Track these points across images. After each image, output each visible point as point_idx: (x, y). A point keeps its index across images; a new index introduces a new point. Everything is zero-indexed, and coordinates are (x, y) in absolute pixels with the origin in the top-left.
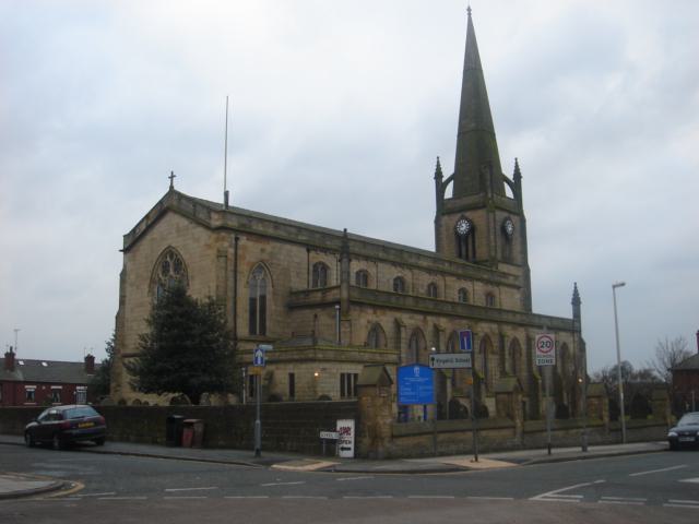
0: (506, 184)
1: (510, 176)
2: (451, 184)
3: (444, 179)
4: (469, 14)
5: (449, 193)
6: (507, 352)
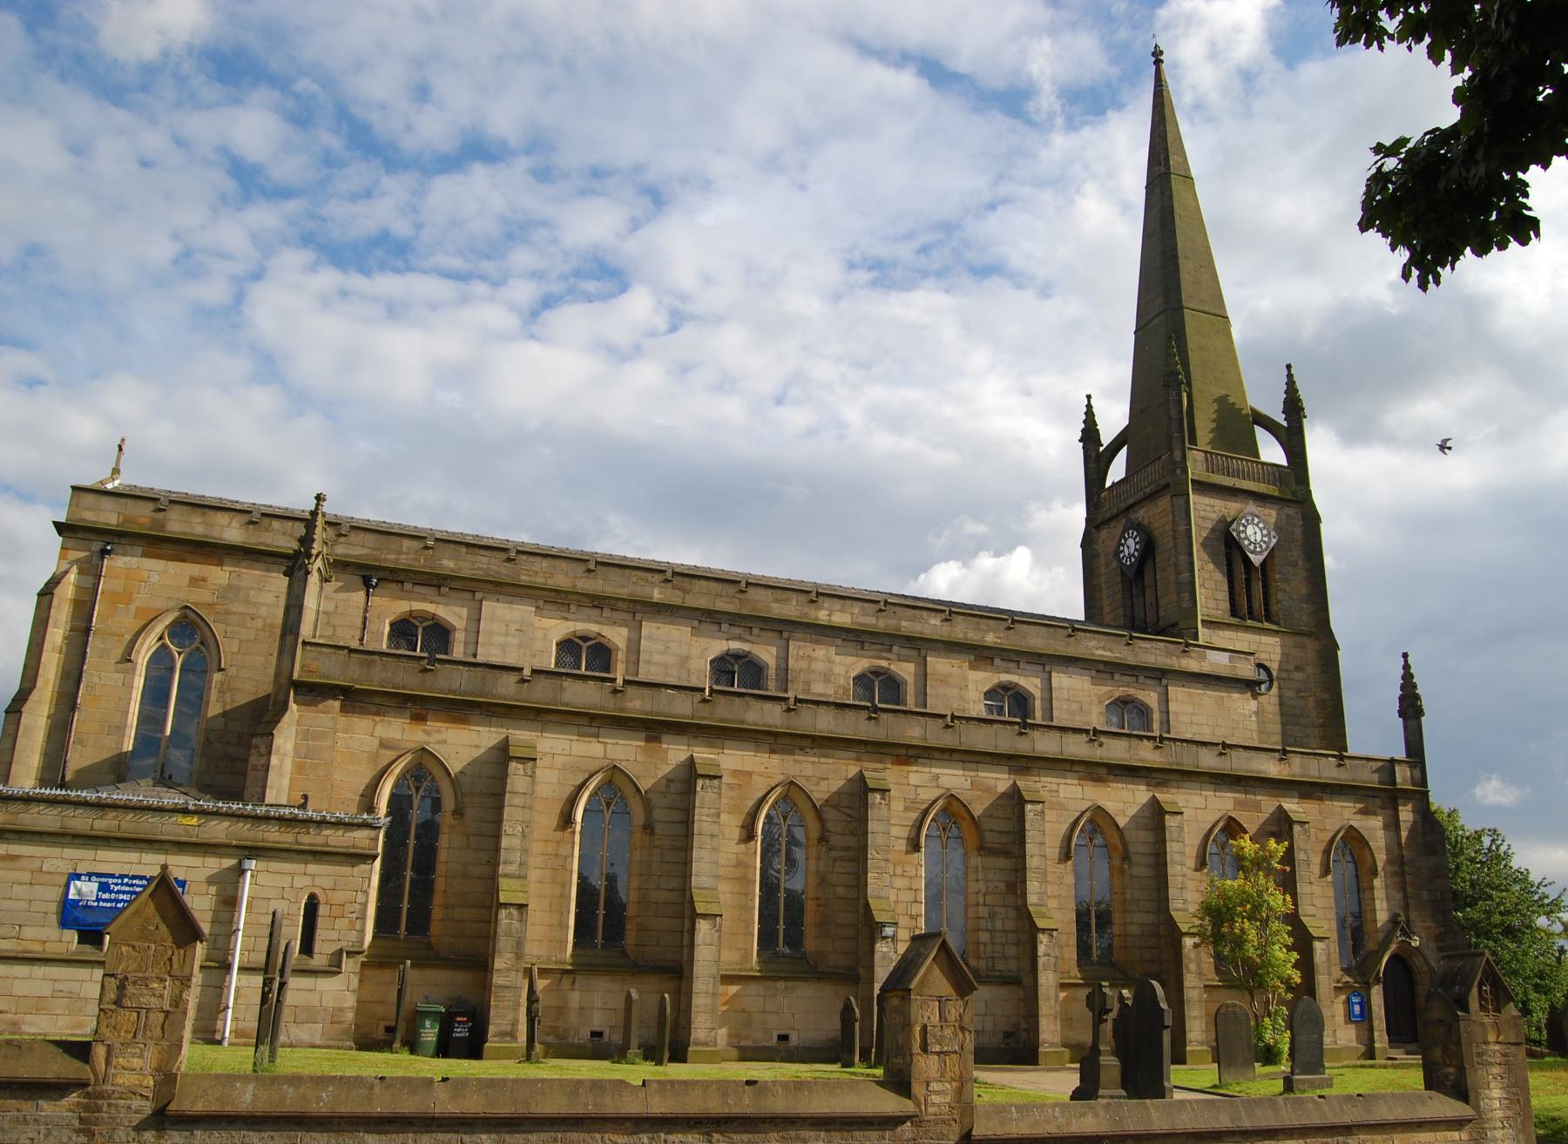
1: (1280, 419)
2: (1124, 450)
5: (1117, 471)
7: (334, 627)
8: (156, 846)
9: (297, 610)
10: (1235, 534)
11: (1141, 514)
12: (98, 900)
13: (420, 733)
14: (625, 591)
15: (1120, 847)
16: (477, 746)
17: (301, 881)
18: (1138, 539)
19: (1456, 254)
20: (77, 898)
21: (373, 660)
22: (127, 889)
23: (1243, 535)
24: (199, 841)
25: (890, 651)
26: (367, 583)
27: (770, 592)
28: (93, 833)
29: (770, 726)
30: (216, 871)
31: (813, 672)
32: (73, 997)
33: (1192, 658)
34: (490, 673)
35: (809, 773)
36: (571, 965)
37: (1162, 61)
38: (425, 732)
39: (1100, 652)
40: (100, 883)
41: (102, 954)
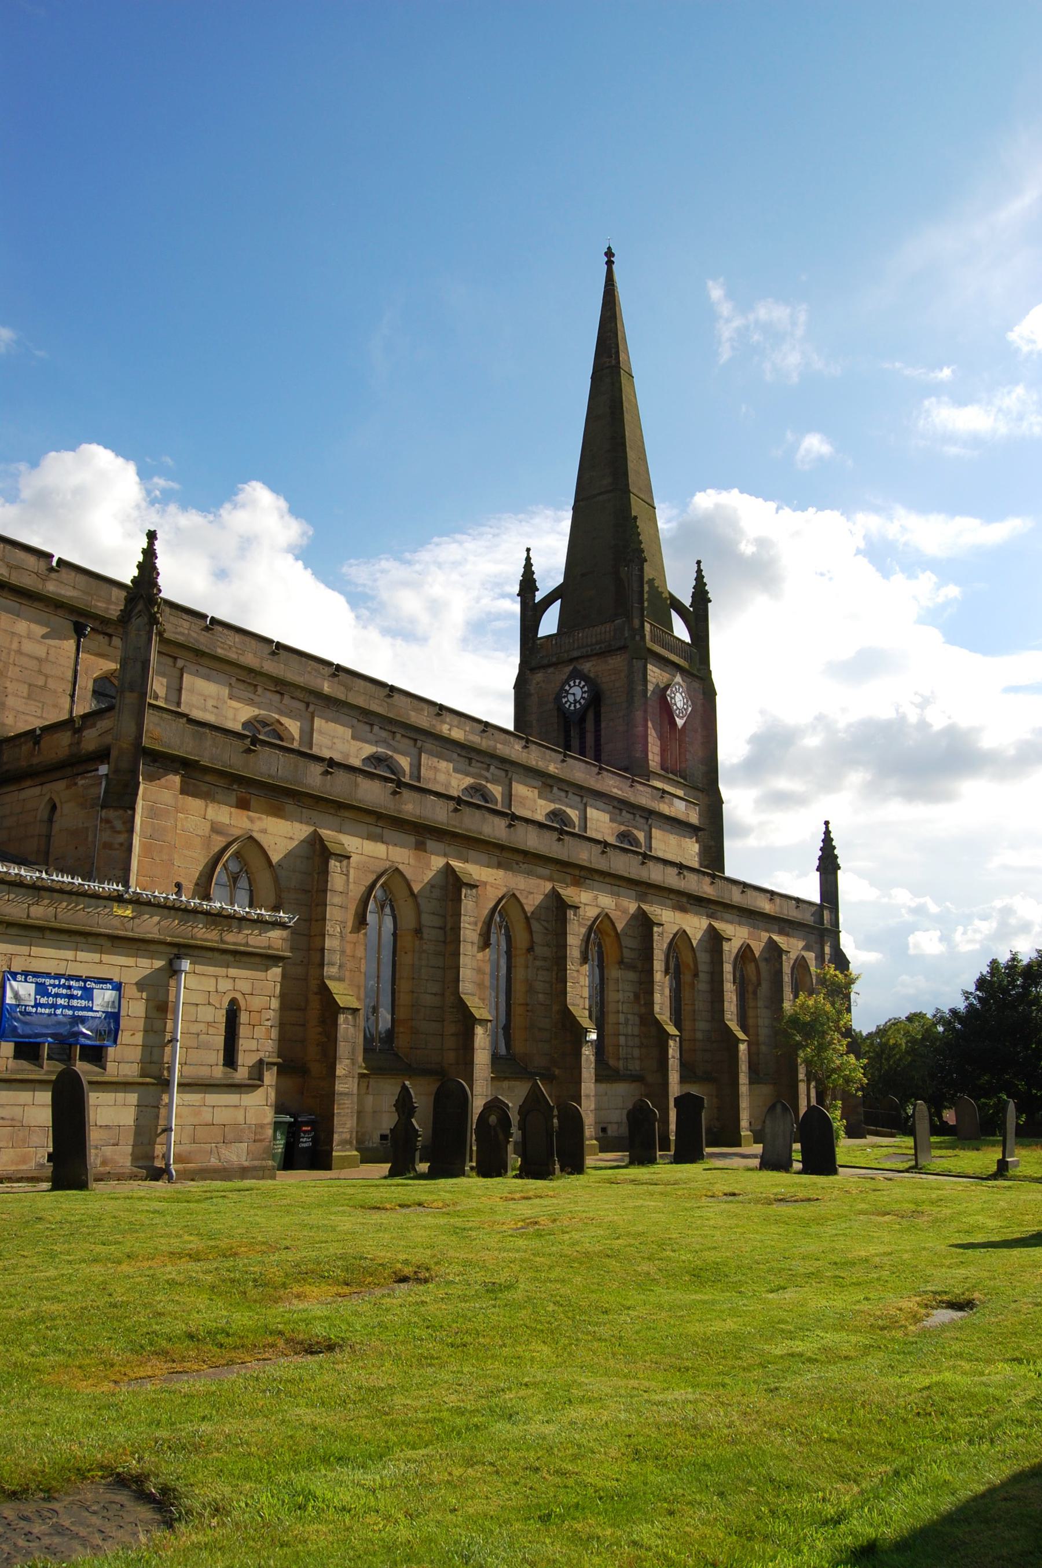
0: (674, 614)
1: (687, 601)
2: (557, 606)
3: (539, 596)
4: (610, 263)
5: (549, 624)
6: (658, 965)
7: (47, 676)
8: (91, 940)
9: (139, 665)
10: (669, 698)
11: (587, 667)
12: (37, 1005)
13: (245, 819)
14: (302, 680)
15: (692, 966)
16: (291, 838)
17: (225, 985)
18: (586, 689)
19: (732, 487)
20: (13, 1002)
21: (204, 733)
22: (64, 991)
23: (673, 701)
24: (136, 935)
25: (488, 770)
26: (79, 631)
27: (409, 700)
28: (30, 921)
29: (499, 839)
30: (149, 971)
31: (438, 782)
32: (16, 1125)
33: (665, 803)
34: (301, 761)
35: (522, 887)
36: (365, 1068)
37: (613, 262)
38: (249, 818)
39: (615, 790)
40: (37, 983)
41: (43, 1072)
